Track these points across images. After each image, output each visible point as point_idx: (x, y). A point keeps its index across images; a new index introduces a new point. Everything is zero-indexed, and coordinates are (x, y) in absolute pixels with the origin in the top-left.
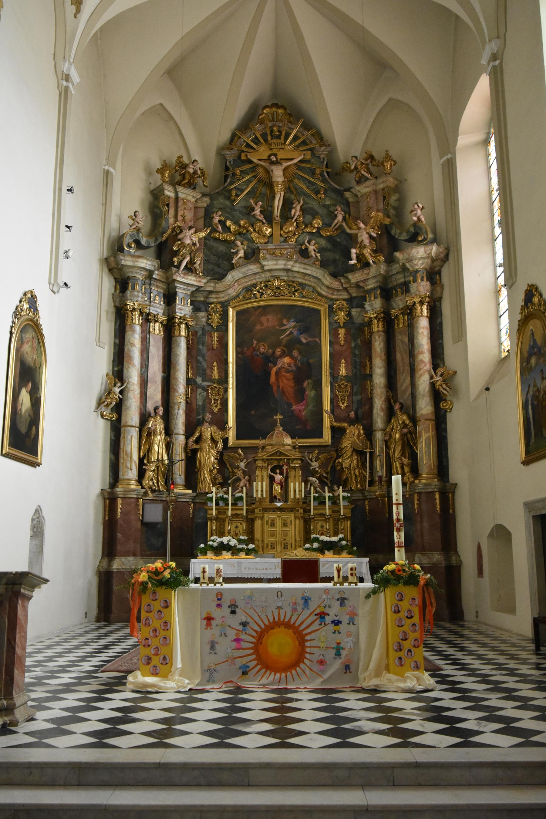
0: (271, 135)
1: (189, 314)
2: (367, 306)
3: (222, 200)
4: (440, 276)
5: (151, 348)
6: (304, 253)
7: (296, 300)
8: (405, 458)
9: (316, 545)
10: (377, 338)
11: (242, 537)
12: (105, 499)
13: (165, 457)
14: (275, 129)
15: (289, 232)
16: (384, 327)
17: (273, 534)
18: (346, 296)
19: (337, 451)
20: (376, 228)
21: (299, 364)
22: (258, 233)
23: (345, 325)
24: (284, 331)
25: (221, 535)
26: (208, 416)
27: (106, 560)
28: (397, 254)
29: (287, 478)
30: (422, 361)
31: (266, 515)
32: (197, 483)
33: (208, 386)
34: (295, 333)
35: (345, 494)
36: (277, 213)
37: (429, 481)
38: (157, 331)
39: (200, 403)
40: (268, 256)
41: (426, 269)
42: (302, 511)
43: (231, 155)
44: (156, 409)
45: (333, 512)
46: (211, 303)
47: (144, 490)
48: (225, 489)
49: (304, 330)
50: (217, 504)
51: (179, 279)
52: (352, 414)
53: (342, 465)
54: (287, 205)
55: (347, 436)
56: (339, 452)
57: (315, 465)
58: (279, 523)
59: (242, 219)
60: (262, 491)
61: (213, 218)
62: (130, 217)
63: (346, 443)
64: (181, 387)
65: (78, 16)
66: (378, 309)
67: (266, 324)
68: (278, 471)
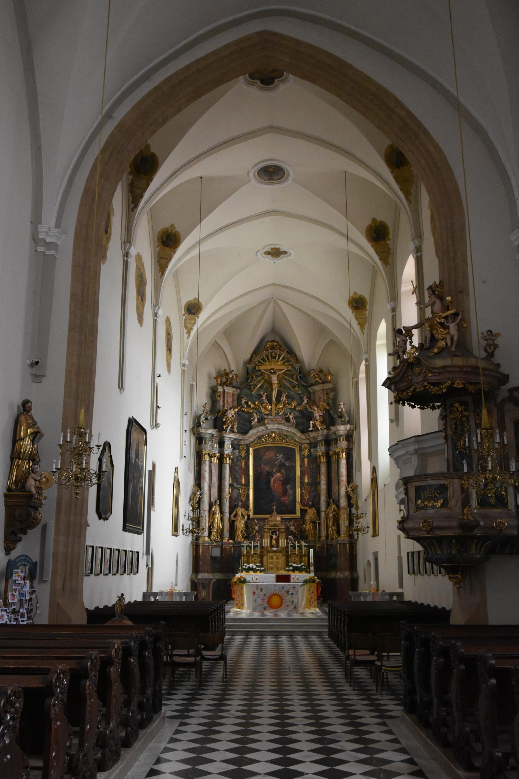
0: (271, 356)
2: (318, 449)
3: (246, 391)
4: (352, 438)
6: (288, 420)
7: (283, 444)
8: (334, 526)
9: (291, 568)
11: (258, 564)
12: (193, 545)
14: (273, 354)
15: (280, 408)
17: (272, 563)
18: (308, 442)
19: (303, 521)
20: (323, 410)
22: (265, 408)
23: (308, 457)
24: (277, 460)
25: (249, 563)
26: (240, 503)
27: (194, 574)
28: (331, 428)
29: (278, 537)
30: (342, 480)
32: (235, 537)
33: (240, 487)
34: (283, 460)
35: (305, 544)
36: (274, 399)
37: (344, 538)
38: (215, 461)
39: (236, 496)
42: (285, 552)
44: (216, 501)
45: (300, 552)
46: (241, 445)
49: (287, 459)
50: (246, 549)
51: (226, 436)
52: (310, 503)
53: (305, 529)
57: (292, 528)
58: (274, 557)
59: (256, 401)
60: (267, 543)
62: (203, 406)
63: (307, 518)
64: (227, 489)
66: (323, 451)
67: (268, 456)
68: (274, 534)
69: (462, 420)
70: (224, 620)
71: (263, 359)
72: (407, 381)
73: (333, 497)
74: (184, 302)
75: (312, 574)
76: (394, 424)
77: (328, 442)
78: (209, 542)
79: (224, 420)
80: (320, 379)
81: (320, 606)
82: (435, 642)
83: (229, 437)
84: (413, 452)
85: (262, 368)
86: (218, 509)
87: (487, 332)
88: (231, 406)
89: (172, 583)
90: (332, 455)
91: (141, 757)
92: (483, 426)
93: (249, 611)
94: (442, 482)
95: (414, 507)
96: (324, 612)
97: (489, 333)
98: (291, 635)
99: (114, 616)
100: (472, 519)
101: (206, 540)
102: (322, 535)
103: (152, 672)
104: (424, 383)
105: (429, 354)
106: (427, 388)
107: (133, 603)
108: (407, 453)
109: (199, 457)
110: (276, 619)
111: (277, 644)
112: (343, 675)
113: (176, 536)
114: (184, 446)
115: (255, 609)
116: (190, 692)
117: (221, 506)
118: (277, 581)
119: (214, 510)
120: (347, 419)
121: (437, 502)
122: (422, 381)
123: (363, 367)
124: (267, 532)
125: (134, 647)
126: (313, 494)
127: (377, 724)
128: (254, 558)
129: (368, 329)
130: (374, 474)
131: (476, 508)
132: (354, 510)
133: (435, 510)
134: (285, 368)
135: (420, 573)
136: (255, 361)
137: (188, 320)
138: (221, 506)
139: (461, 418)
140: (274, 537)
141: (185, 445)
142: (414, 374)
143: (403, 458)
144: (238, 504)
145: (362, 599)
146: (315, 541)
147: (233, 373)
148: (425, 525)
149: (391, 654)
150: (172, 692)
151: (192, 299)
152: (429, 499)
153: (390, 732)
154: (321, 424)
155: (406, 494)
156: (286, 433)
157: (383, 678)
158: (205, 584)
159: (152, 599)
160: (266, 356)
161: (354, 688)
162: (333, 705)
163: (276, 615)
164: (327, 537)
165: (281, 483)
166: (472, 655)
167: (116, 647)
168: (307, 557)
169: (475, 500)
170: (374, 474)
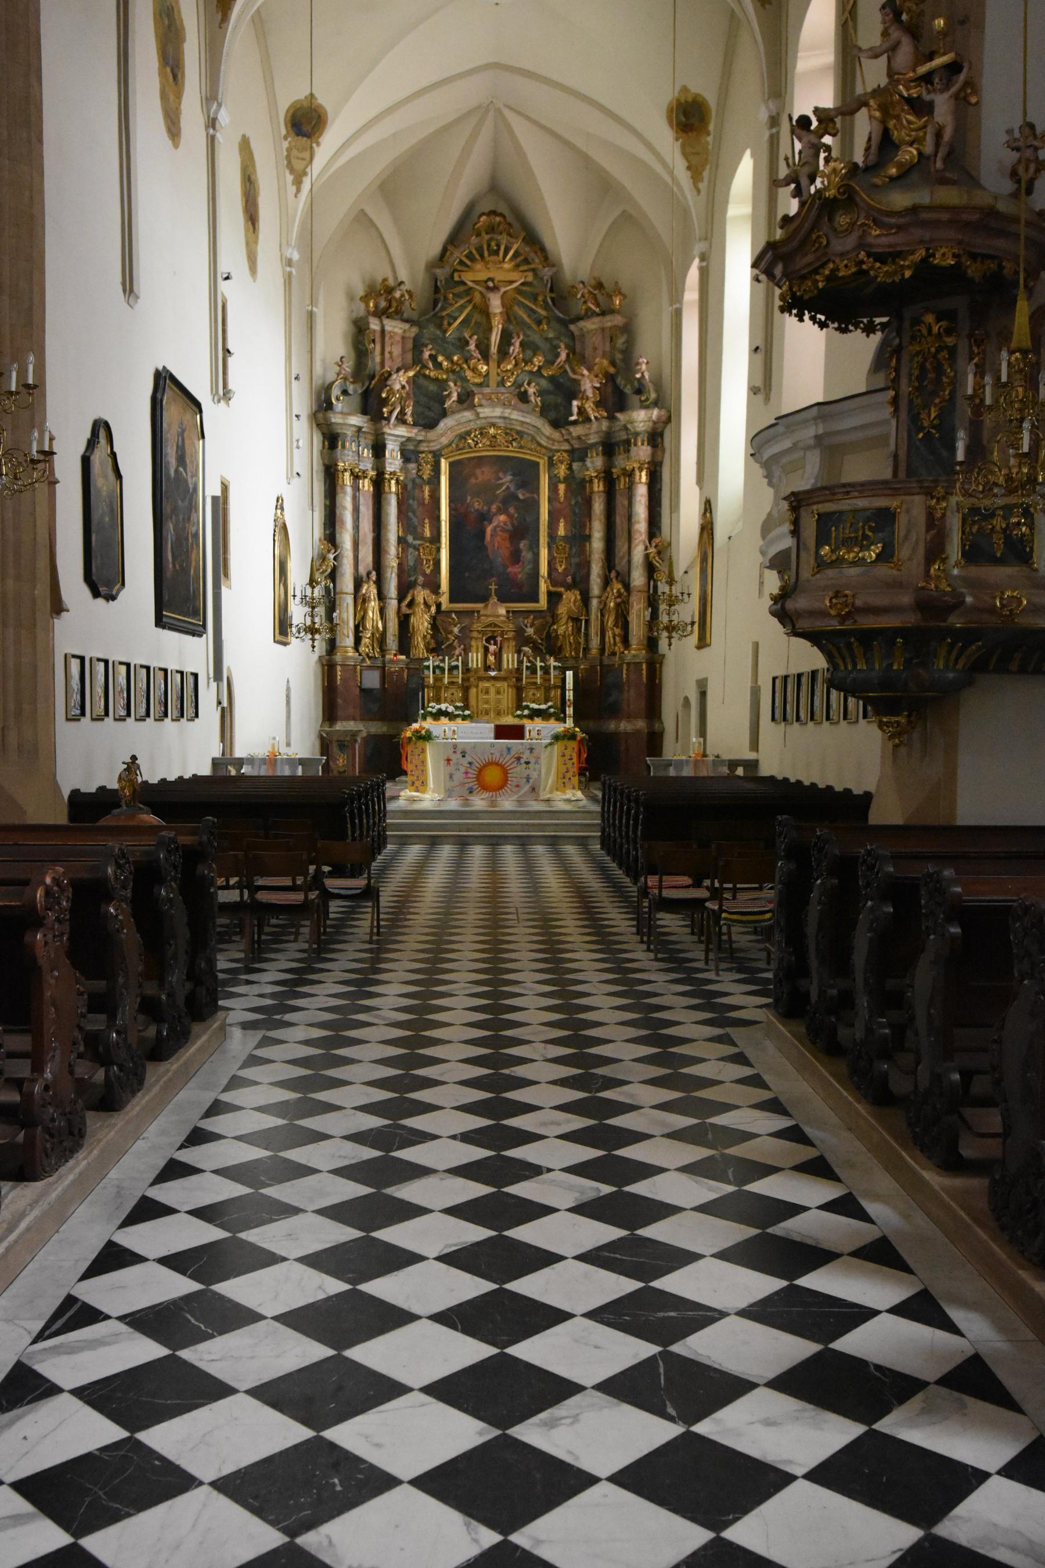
0: (488, 250)
1: (399, 467)
2: (588, 463)
5: (361, 507)
6: (523, 397)
7: (512, 451)
8: (617, 627)
9: (526, 712)
10: (597, 499)
12: (323, 665)
13: (380, 625)
14: (493, 244)
15: (507, 371)
16: (605, 487)
17: (487, 702)
18: (566, 447)
19: (552, 617)
20: (600, 375)
21: (516, 524)
23: (566, 480)
24: (502, 485)
25: (438, 701)
28: (618, 415)
29: (500, 649)
31: (480, 684)
33: (420, 545)
34: (512, 489)
35: (556, 664)
36: (494, 349)
38: (366, 488)
39: (411, 563)
40: (484, 402)
41: (648, 432)
42: (514, 680)
43: (441, 273)
44: (369, 574)
46: (422, 452)
47: (361, 657)
48: (441, 657)
49: (523, 485)
50: (434, 672)
52: (569, 579)
54: (506, 338)
55: (564, 602)
56: (555, 618)
57: (530, 631)
58: (492, 691)
59: (455, 354)
61: (422, 352)
62: (337, 363)
63: (562, 610)
65: (299, 195)
66: (599, 468)
68: (492, 642)
69: (939, 356)
70: (383, 813)
71: (470, 257)
72: (815, 251)
73: (618, 568)
74: (284, 106)
75: (570, 723)
76: (760, 397)
77: (610, 447)
78: (357, 659)
79: (384, 395)
80: (598, 305)
81: (584, 787)
82: (874, 866)
83: (396, 434)
84: (812, 442)
85: (468, 277)
86: (373, 591)
87: (1020, 128)
88: (400, 365)
89: (274, 738)
90: (618, 477)
91: (153, 1128)
92: (1014, 345)
93: (437, 797)
94: (881, 502)
95: (812, 562)
96: (593, 799)
97: (1027, 130)
98: (523, 843)
99: (119, 806)
100: (949, 589)
101: (350, 654)
102: (591, 646)
103: (183, 934)
104: (857, 255)
105: (878, 181)
106: (864, 267)
107: (190, 779)
108: (795, 445)
109: (331, 475)
110: (491, 812)
111: (494, 864)
112: (632, 926)
113: (285, 644)
114: (295, 451)
115: (449, 793)
116: (294, 965)
117: (379, 583)
118: (497, 737)
119: (366, 593)
120: (653, 396)
121: (869, 550)
122: (854, 249)
123: (693, 275)
124: (476, 639)
125: (117, 879)
126: (575, 560)
127: (711, 1040)
128: (450, 692)
129: (709, 181)
130: (708, 515)
131: (957, 564)
132: (663, 587)
133: (864, 569)
134: (519, 279)
135: (798, 719)
136: (451, 260)
137: (295, 152)
138: (379, 583)
139: (938, 351)
140: (492, 648)
141: (298, 447)
142: (835, 230)
143: (784, 460)
144: (416, 580)
145: (672, 772)
146: (576, 658)
147: (404, 288)
148: (836, 604)
149: (738, 886)
150: (257, 966)
151: (303, 97)
152: (849, 543)
153: (740, 1059)
154: (597, 407)
155: (795, 532)
156: (519, 428)
157: (720, 934)
158: (345, 744)
159: (233, 773)
160: (477, 249)
161: (656, 955)
162: (605, 982)
163: (493, 803)
164: (602, 650)
165: (506, 535)
166: (989, 901)
167: (48, 880)
168: (559, 691)
169: (956, 546)
170: (708, 515)
